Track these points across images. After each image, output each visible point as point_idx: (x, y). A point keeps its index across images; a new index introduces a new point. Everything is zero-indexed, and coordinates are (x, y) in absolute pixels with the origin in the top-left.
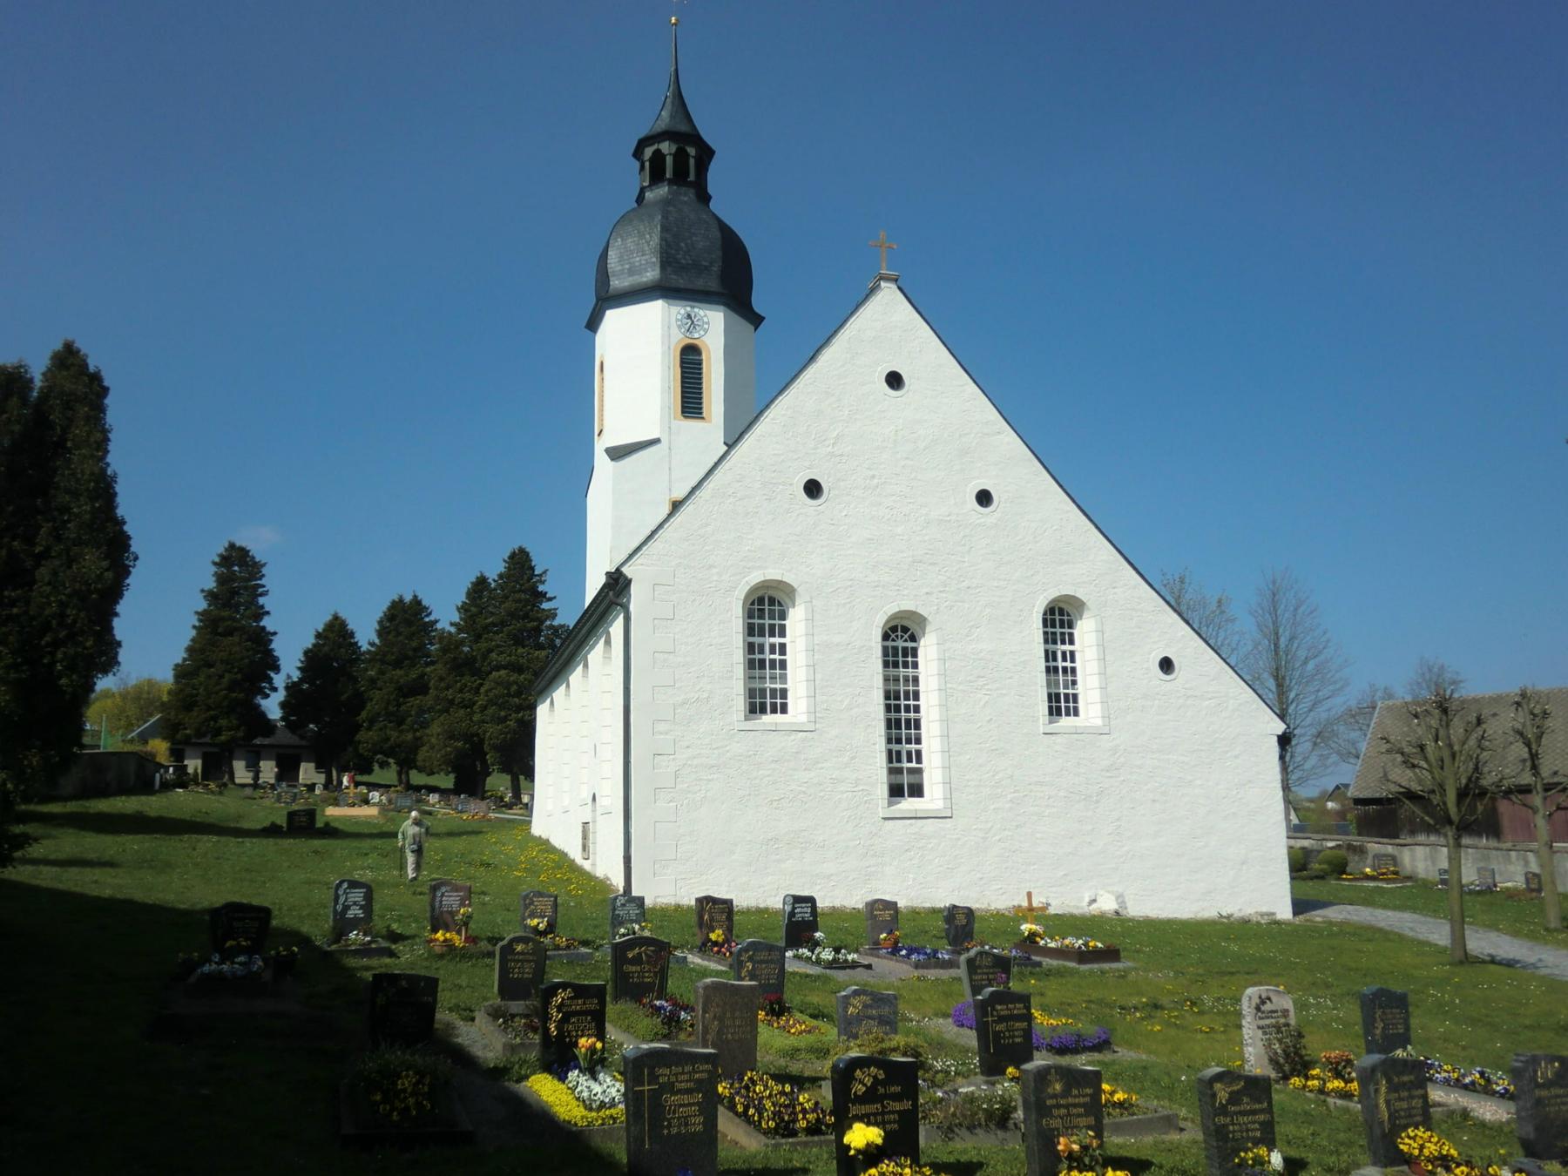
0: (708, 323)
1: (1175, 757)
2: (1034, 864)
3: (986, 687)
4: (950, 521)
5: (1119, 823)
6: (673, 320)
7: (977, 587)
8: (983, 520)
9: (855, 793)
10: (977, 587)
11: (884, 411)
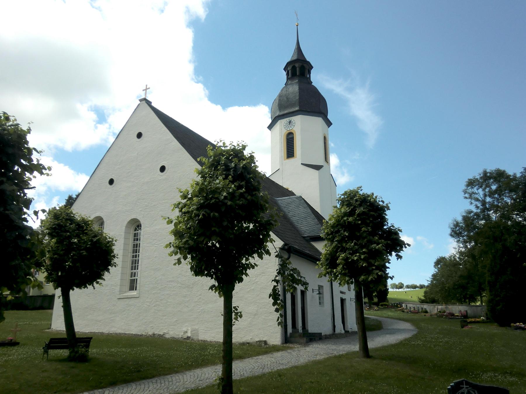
0: (295, 123)
2: (165, 316)
3: (156, 244)
5: (200, 297)
9: (110, 290)
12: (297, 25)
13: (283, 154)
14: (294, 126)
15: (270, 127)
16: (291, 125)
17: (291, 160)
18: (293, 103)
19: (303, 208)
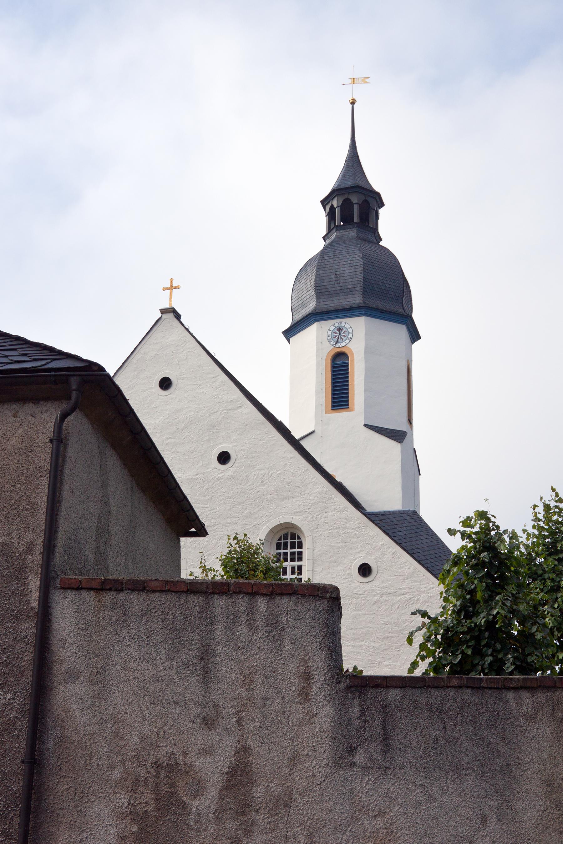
0: (352, 333)
1: (367, 644)
4: (198, 478)
6: (325, 336)
7: (215, 525)
8: (221, 475)
10: (215, 525)
11: (156, 407)
12: (353, 103)
13: (324, 399)
14: (351, 339)
15: (289, 333)
16: (344, 336)
17: (341, 416)
18: (349, 287)
19: (427, 537)
